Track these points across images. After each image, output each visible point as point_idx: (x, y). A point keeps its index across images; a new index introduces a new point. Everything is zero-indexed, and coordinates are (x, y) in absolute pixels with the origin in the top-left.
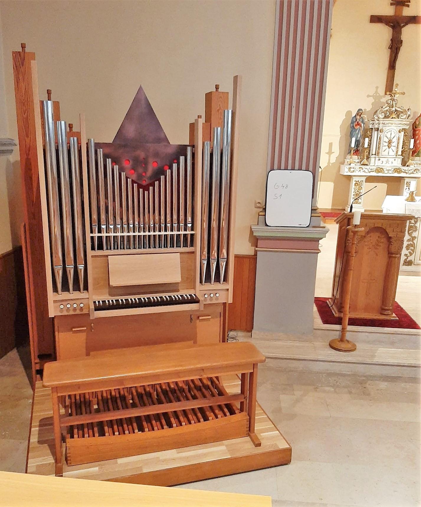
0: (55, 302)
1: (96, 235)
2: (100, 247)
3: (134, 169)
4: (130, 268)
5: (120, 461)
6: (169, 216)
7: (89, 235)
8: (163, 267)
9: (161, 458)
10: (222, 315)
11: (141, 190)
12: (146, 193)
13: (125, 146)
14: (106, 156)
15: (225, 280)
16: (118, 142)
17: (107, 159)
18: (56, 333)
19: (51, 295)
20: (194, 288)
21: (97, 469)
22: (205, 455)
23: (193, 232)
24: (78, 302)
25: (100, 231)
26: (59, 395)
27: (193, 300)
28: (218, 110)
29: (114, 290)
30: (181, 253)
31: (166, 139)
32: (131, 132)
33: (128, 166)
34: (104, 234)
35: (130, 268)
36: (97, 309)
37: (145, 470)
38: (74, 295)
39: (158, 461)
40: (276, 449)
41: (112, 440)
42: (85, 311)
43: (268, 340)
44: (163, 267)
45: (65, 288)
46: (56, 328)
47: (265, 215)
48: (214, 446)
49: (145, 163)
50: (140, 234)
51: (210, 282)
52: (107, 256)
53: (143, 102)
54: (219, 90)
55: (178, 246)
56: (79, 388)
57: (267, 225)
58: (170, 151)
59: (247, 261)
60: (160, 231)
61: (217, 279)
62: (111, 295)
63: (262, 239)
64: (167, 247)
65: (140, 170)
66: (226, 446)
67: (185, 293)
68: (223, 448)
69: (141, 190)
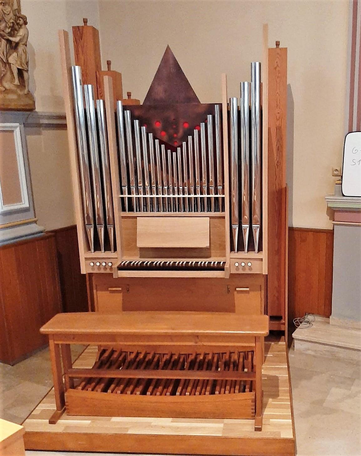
0: (86, 259)
1: (126, 196)
2: (131, 209)
3: (165, 129)
4: (159, 230)
5: (115, 419)
6: (204, 179)
7: (117, 196)
8: (191, 230)
9: (152, 424)
10: (263, 287)
11: (169, 151)
12: (174, 153)
13: (155, 108)
14: (133, 118)
15: (260, 249)
16: (148, 103)
17: (135, 121)
18: (95, 291)
19: (83, 253)
20: (224, 256)
21: (89, 422)
22: (197, 429)
23: (223, 196)
24: (107, 261)
25: (129, 193)
26: (56, 342)
27: (220, 268)
28: (275, 68)
29: (145, 251)
30: (211, 217)
31: (196, 99)
32: (160, 93)
33: (158, 126)
34: (134, 196)
35: (159, 230)
36: (121, 268)
37: (130, 432)
38: (102, 254)
39: (149, 426)
40: (277, 437)
41: (113, 397)
42: (108, 271)
43: (348, 328)
44: (191, 230)
45: (97, 248)
46: (94, 286)
47: (342, 184)
48: (213, 422)
49: (176, 123)
50: (179, 196)
51: (244, 251)
52: (136, 217)
53: (171, 61)
54: (280, 46)
55: (209, 210)
56: (74, 339)
57: (344, 196)
58: (200, 110)
59: (324, 237)
60: (195, 194)
61: (251, 247)
62: (141, 257)
63: (339, 211)
64: (197, 211)
65: (171, 131)
66: (225, 424)
67: (214, 260)
68: (221, 425)
69: (169, 151)
